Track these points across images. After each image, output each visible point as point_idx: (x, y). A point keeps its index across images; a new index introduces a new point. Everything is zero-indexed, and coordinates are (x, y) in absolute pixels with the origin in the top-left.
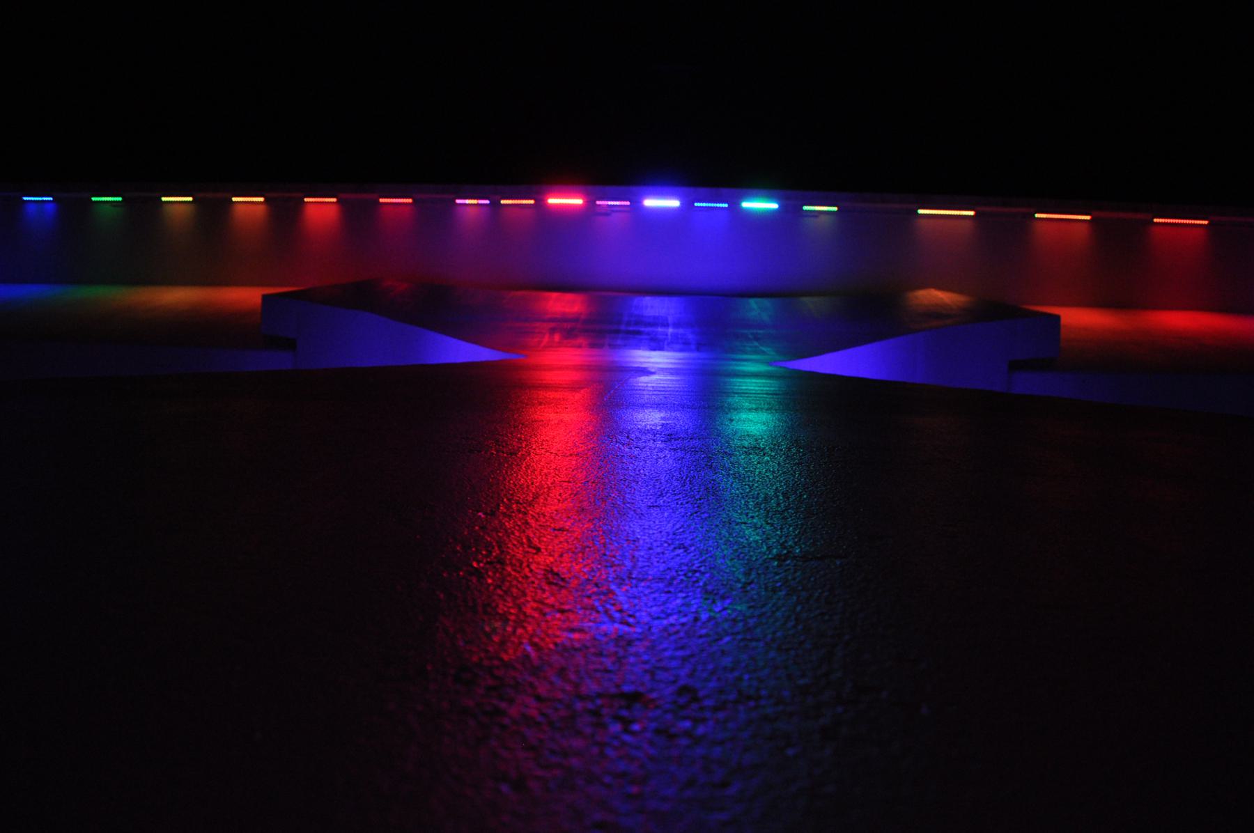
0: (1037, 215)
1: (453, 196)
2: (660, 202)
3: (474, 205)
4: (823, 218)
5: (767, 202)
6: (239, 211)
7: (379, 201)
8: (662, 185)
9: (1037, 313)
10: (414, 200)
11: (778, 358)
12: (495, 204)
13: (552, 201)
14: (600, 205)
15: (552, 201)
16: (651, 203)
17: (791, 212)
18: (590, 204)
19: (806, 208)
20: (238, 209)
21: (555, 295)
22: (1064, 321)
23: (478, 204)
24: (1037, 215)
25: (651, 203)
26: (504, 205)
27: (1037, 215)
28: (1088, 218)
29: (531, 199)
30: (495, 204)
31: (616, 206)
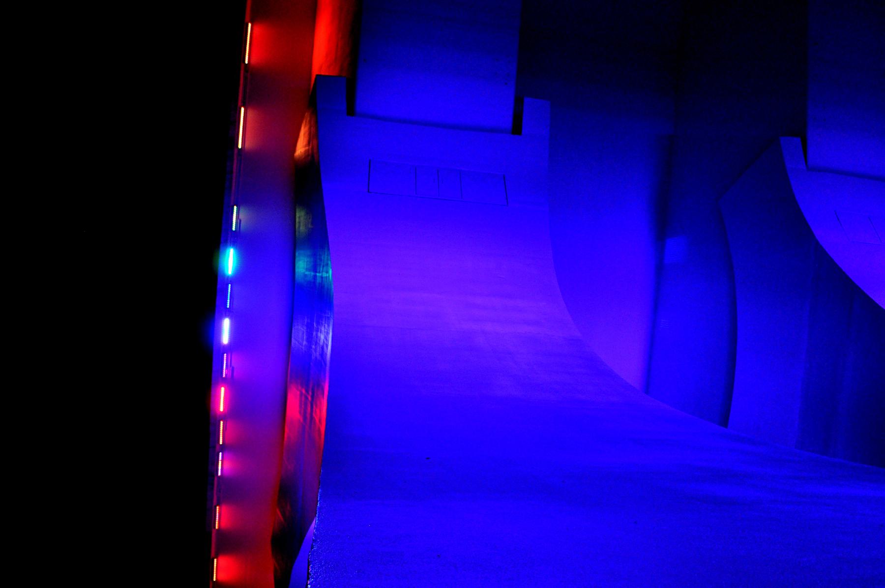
0: (246, 62)
1: (211, 582)
2: (226, 330)
3: (222, 463)
4: (241, 216)
5: (229, 257)
6: (224, 577)
7: (220, 476)
8: (213, 330)
9: (313, 88)
10: (218, 505)
11: (326, 249)
12: (223, 448)
13: (222, 409)
14: (226, 375)
15: (222, 409)
16: (225, 339)
17: (237, 239)
18: (225, 381)
19: (234, 229)
20: (253, 61)
21: (297, 270)
22: (317, 73)
23: (222, 461)
24: (246, 62)
25: (225, 339)
26: (223, 442)
27: (246, 62)
28: (250, 25)
29: (214, 561)
30: (223, 448)
31: (226, 363)
